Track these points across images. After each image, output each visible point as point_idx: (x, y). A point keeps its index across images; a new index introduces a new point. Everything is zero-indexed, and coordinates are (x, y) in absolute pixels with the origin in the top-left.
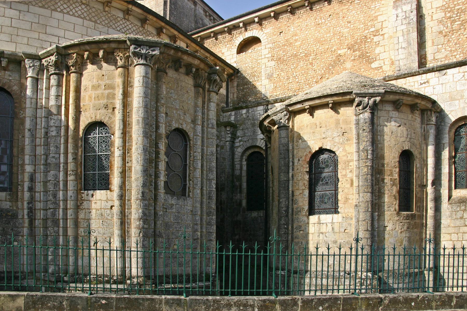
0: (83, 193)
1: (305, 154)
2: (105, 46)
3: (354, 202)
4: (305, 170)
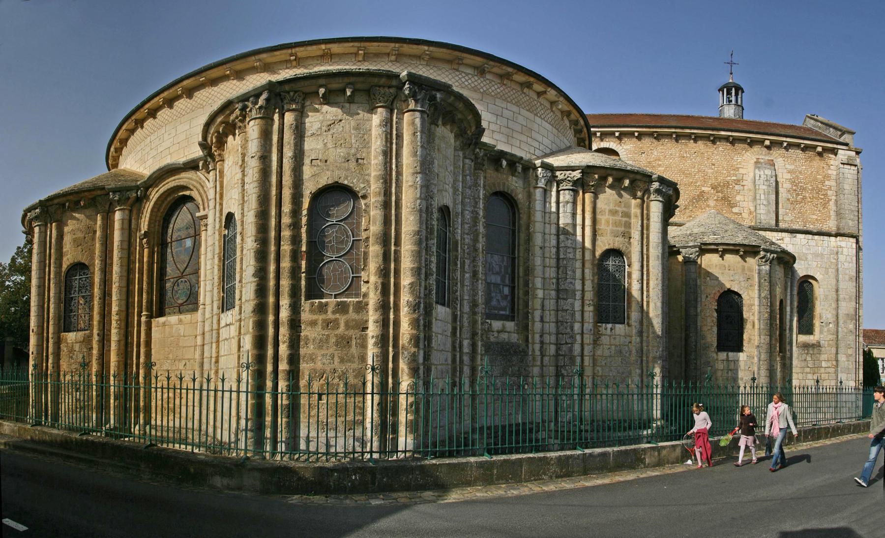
0: (600, 326)
1: (714, 292)
2: (632, 176)
3: (756, 343)
4: (713, 307)
